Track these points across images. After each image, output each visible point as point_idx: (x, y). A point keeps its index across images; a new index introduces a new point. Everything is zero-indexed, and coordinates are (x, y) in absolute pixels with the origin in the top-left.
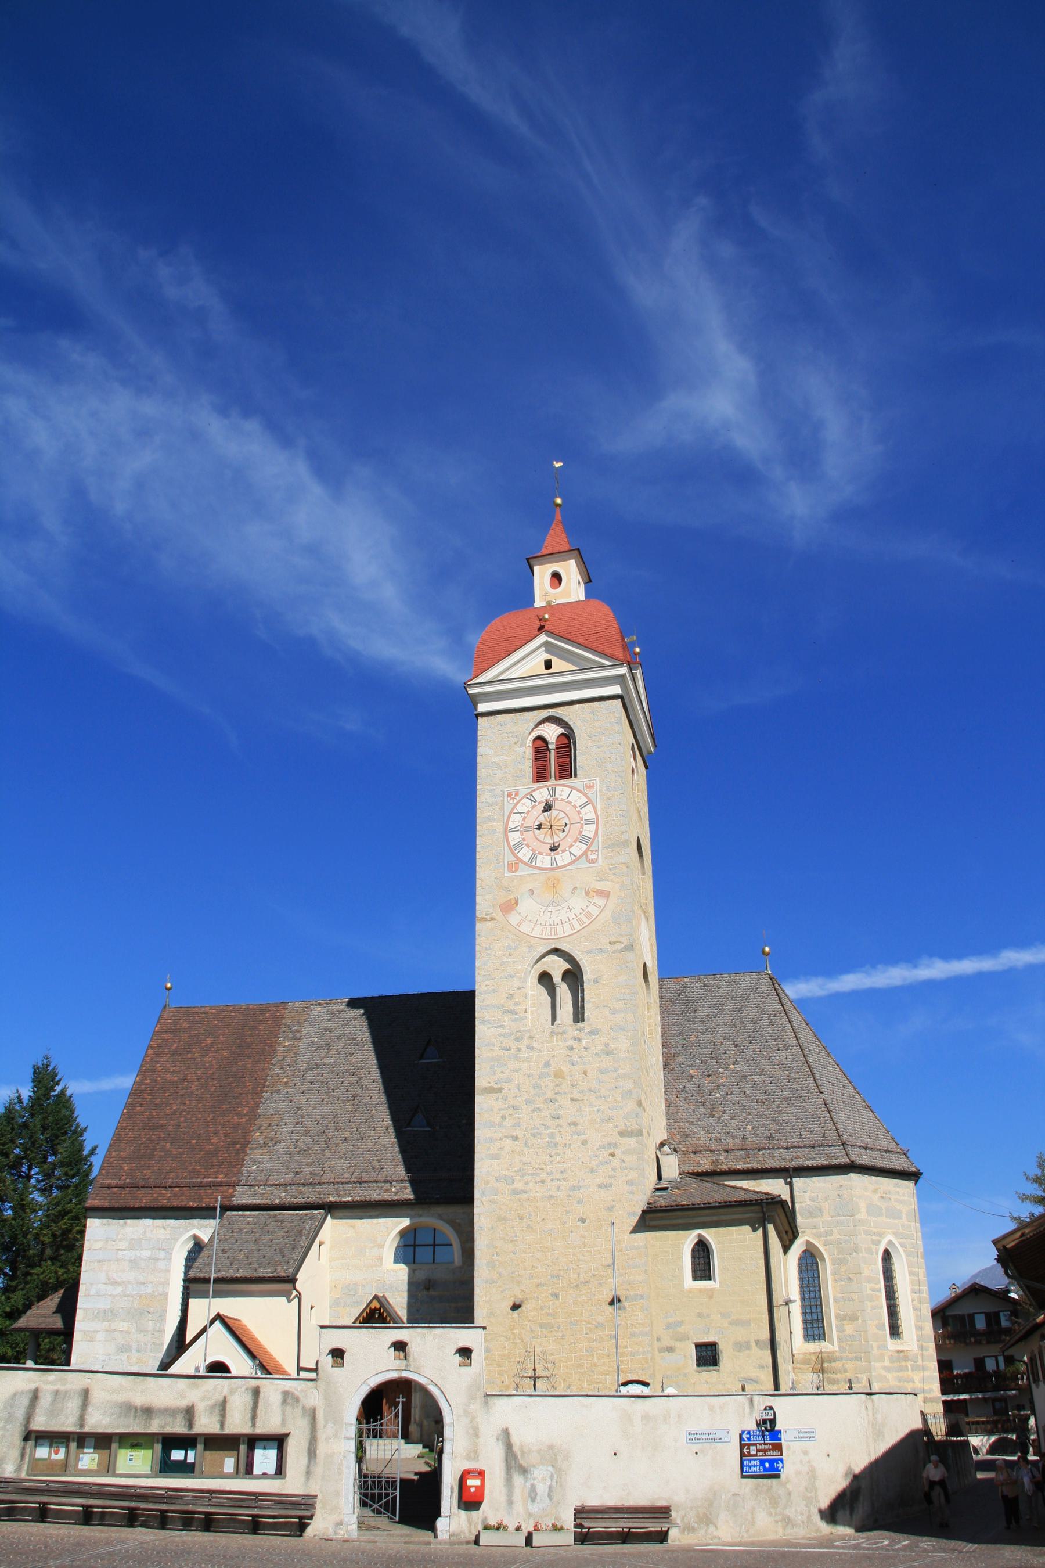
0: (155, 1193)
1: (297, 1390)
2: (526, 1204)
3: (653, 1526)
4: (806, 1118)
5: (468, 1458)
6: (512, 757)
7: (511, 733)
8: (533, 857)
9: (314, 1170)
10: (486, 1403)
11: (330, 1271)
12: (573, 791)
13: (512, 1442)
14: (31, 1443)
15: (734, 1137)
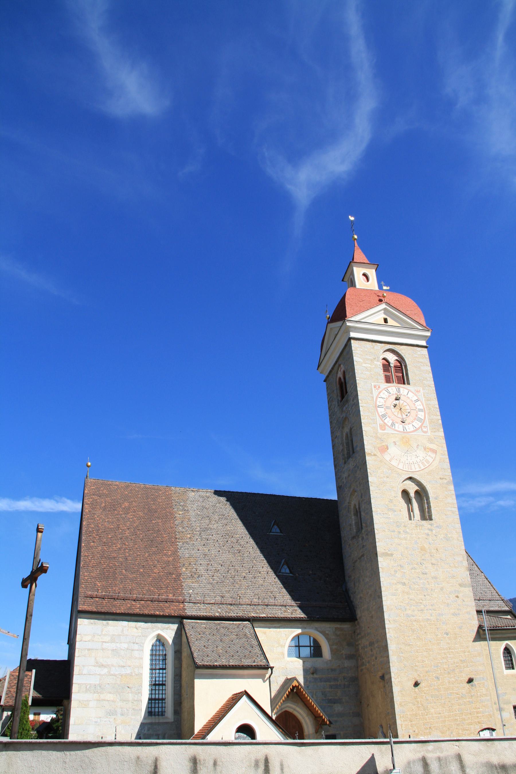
0: (129, 604)
8: (393, 424)
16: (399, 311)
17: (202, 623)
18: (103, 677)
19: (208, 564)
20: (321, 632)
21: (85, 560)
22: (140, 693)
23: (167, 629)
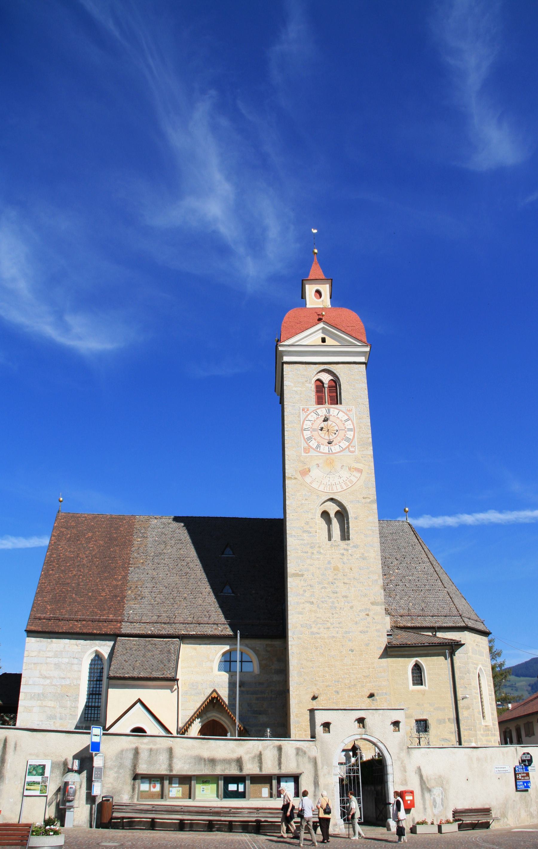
0: (71, 624)
1: (304, 747)
2: (319, 640)
3: (483, 820)
4: (440, 601)
5: (402, 784)
6: (304, 389)
7: (303, 375)
8: (318, 446)
9: (169, 615)
10: (408, 752)
11: (182, 675)
12: (340, 412)
13: (422, 774)
14: (138, 781)
15: (404, 609)
16: (337, 328)
17: (133, 641)
18: (46, 686)
19: (154, 587)
20: (251, 648)
21: (42, 586)
22: (77, 701)
23: (104, 645)
